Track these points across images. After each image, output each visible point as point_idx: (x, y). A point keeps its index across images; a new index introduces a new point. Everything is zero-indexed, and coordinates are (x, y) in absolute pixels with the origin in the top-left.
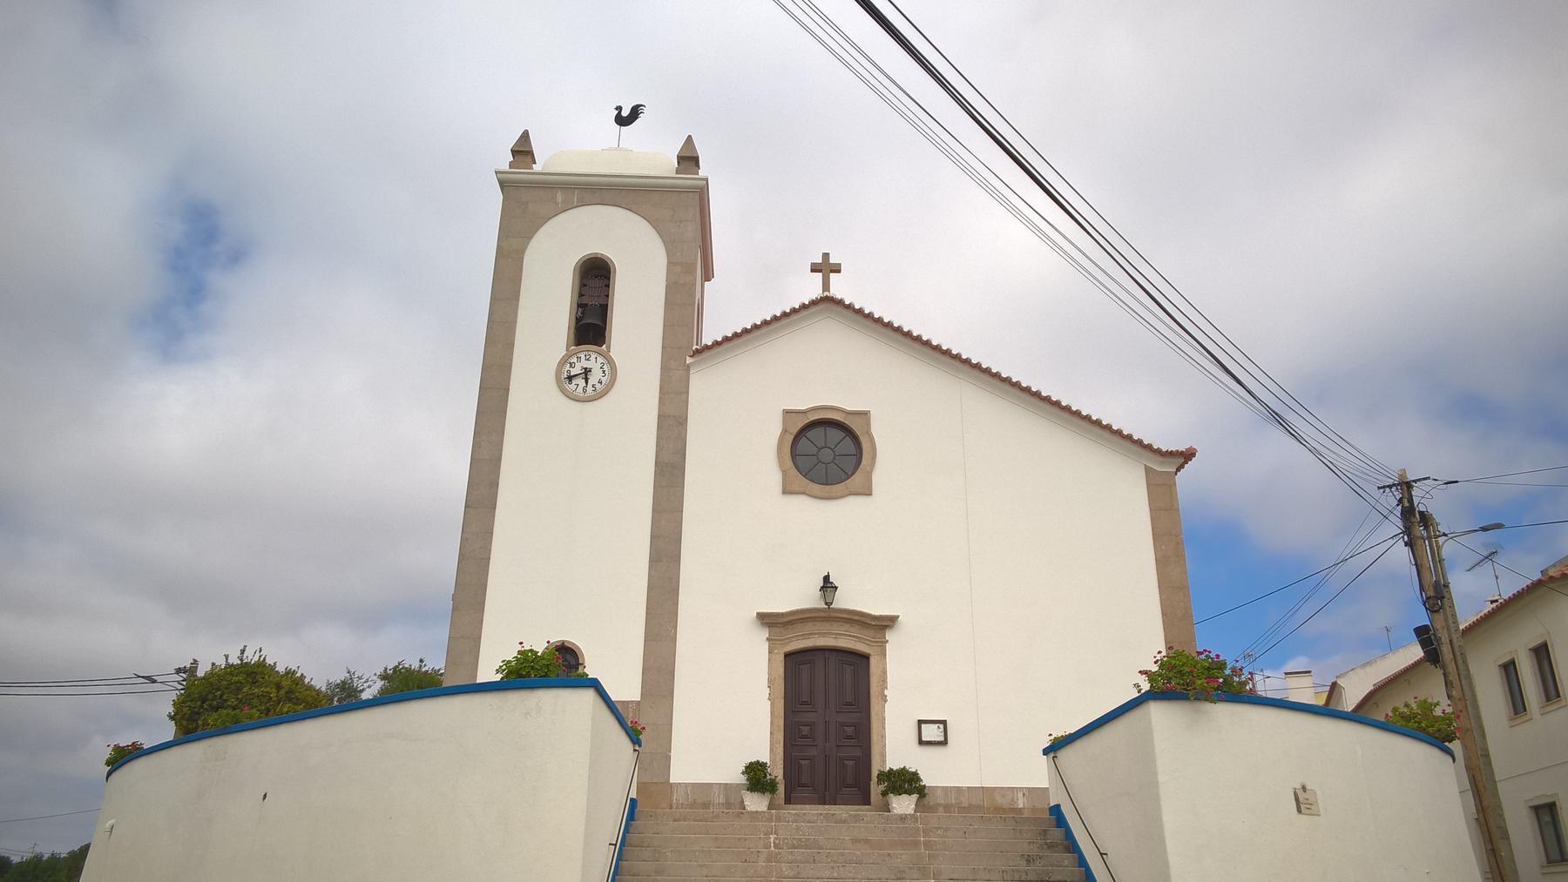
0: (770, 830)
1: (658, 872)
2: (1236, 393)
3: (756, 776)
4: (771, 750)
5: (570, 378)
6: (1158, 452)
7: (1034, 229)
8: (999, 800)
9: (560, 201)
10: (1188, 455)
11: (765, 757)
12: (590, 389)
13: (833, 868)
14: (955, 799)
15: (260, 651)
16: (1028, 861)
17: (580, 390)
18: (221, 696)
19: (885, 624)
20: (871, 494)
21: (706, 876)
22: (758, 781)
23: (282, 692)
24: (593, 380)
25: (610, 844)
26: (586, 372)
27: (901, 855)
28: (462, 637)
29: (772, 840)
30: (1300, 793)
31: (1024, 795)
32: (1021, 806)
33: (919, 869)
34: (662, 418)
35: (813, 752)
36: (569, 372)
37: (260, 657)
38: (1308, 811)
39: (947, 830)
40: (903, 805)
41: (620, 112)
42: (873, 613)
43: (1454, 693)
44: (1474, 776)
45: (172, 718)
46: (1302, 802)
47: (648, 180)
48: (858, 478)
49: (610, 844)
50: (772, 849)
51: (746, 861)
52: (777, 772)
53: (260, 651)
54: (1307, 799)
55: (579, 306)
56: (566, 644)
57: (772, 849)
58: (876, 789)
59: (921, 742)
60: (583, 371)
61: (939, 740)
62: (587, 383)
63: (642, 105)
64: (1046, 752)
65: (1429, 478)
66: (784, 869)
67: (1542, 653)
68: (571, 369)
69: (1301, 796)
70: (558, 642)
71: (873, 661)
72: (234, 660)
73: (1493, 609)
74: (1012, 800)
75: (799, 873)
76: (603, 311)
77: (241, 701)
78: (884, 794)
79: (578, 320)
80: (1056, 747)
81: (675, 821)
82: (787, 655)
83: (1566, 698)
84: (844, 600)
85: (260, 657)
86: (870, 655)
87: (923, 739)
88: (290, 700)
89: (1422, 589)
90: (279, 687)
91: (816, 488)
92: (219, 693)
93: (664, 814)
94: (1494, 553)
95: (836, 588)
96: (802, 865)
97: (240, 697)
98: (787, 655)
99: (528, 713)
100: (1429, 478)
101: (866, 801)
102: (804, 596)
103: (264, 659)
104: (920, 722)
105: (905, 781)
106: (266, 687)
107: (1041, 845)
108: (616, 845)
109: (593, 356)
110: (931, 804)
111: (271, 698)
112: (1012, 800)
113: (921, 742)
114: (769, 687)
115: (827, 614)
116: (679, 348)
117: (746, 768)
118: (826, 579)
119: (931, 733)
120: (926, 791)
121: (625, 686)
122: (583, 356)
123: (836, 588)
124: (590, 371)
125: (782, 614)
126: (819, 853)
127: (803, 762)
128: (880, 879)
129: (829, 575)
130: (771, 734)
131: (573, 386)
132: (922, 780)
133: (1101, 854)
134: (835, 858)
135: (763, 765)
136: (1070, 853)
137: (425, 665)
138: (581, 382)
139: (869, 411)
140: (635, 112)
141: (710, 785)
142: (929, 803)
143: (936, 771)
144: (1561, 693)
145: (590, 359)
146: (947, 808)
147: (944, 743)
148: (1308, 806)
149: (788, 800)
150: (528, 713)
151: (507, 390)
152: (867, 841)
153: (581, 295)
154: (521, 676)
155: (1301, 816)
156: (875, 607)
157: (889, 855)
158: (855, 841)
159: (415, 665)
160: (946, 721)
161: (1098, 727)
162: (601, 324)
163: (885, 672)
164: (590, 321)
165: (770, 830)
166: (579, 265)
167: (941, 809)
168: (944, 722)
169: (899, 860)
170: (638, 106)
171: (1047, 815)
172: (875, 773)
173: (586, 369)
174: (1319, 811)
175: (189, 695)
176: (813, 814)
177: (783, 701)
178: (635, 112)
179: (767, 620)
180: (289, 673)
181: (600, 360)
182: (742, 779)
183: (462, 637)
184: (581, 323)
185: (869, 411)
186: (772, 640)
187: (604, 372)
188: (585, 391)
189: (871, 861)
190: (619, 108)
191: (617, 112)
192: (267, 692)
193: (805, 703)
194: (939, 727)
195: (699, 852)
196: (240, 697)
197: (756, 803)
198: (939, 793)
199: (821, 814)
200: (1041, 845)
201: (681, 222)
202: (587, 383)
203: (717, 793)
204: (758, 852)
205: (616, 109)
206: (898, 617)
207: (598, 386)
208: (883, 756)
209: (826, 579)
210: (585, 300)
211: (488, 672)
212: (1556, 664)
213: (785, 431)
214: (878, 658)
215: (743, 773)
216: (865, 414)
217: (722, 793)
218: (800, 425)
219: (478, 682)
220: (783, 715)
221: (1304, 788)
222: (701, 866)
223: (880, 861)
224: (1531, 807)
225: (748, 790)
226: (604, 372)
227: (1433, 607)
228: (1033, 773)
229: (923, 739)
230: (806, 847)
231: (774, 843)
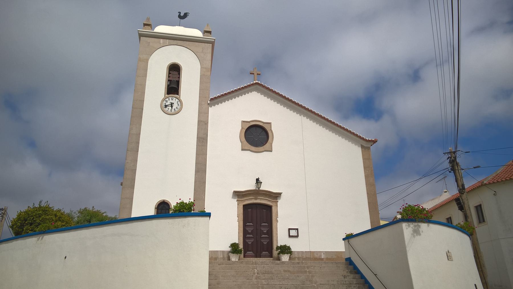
0: (254, 268)
1: (218, 284)
3: (234, 248)
4: (239, 239)
5: (166, 106)
6: (366, 140)
7: (435, 34)
8: (316, 256)
9: (162, 43)
10: (375, 142)
11: (237, 242)
12: (173, 110)
13: (280, 281)
14: (301, 255)
15: (47, 202)
16: (344, 277)
17: (169, 110)
18: (33, 219)
19: (276, 196)
20: (271, 151)
21: (235, 285)
22: (236, 250)
23: (57, 217)
24: (175, 106)
26: (172, 104)
27: (302, 276)
28: (126, 198)
29: (256, 271)
30: (448, 253)
31: (324, 254)
32: (323, 257)
33: (310, 281)
34: (199, 122)
37: (47, 204)
39: (315, 266)
40: (285, 258)
41: (180, 14)
42: (274, 192)
43: (469, 220)
44: (476, 248)
45: (459, 210)
46: (449, 257)
47: (191, 38)
48: (267, 145)
50: (256, 274)
51: (248, 279)
52: (241, 246)
53: (47, 202)
54: (450, 255)
55: (169, 80)
56: (165, 201)
57: (256, 274)
58: (275, 253)
59: (290, 236)
60: (171, 103)
61: (295, 235)
62: (172, 108)
63: (188, 13)
64: (344, 239)
65: (460, 151)
66: (263, 282)
68: (166, 103)
69: (448, 254)
70: (162, 200)
71: (274, 208)
72: (37, 206)
74: (320, 255)
75: (268, 283)
76: (178, 83)
77: (41, 221)
78: (279, 254)
79: (168, 86)
80: (348, 238)
81: (219, 265)
82: (244, 206)
83: (487, 222)
84: (264, 187)
85: (47, 204)
86: (272, 206)
87: (291, 235)
88: (60, 221)
89: (458, 186)
90: (56, 216)
91: (253, 148)
92: (32, 218)
93: (215, 263)
94: (445, 177)
95: (262, 183)
96: (269, 280)
97: (40, 219)
98: (244, 206)
99: (184, 226)
100: (460, 151)
101: (271, 256)
102: (251, 186)
103: (49, 205)
104: (289, 229)
105: (285, 249)
106: (51, 215)
107: (347, 272)
109: (174, 99)
110: (293, 257)
111: (53, 220)
112: (320, 255)
113: (290, 236)
114: (238, 217)
115: (257, 192)
116: (205, 97)
117: (231, 245)
118: (257, 180)
119: (293, 233)
120: (293, 253)
122: (171, 99)
123: (262, 183)
124: (173, 104)
125: (243, 191)
126: (274, 276)
128: (297, 285)
130: (238, 233)
131: (167, 109)
132: (291, 249)
133: (375, 275)
134: (279, 278)
135: (238, 244)
136: (357, 274)
137: (95, 209)
138: (170, 108)
139: (271, 123)
140: (186, 15)
141: (217, 251)
142: (292, 257)
143: (296, 246)
144: (486, 221)
145: (172, 99)
146: (299, 258)
149: (244, 257)
150: (184, 226)
151: (143, 109)
152: (289, 271)
153: (169, 77)
154: (181, 212)
155: (449, 261)
156: (274, 190)
157: (298, 276)
158: (285, 271)
159: (91, 209)
160: (298, 229)
161: (29, 236)
162: (176, 87)
163: (277, 212)
164: (173, 86)
165: (254, 268)
167: (297, 259)
168: (297, 229)
169: (301, 278)
170: (187, 13)
171: (344, 261)
172: (275, 247)
173: (172, 103)
174: (453, 259)
175: (19, 219)
176: (268, 262)
177: (243, 222)
178: (186, 15)
179: (238, 195)
180: (59, 211)
181: (177, 100)
182: (229, 249)
183: (126, 198)
185: (271, 123)
186: (239, 200)
187: (178, 104)
188: (171, 111)
189: (292, 278)
190: (180, 13)
191: (179, 14)
192: (52, 218)
194: (296, 231)
195: (231, 276)
196: (40, 219)
197: (234, 258)
198: (296, 253)
199: (271, 262)
200: (347, 272)
201: (205, 53)
202: (172, 108)
203: (220, 254)
204: (252, 276)
205: (179, 12)
206: (282, 193)
207: (176, 109)
208: (277, 241)
209: (257, 180)
210: (170, 79)
212: (484, 211)
213: (242, 128)
214: (275, 207)
215: (229, 247)
216: (270, 123)
217: (221, 254)
218: (248, 126)
219: (132, 217)
220: (243, 226)
221: (448, 251)
222: (234, 281)
223: (295, 278)
225: (232, 253)
226: (178, 104)
227: (462, 192)
228: (340, 247)
229: (291, 235)
230: (268, 274)
231: (257, 272)
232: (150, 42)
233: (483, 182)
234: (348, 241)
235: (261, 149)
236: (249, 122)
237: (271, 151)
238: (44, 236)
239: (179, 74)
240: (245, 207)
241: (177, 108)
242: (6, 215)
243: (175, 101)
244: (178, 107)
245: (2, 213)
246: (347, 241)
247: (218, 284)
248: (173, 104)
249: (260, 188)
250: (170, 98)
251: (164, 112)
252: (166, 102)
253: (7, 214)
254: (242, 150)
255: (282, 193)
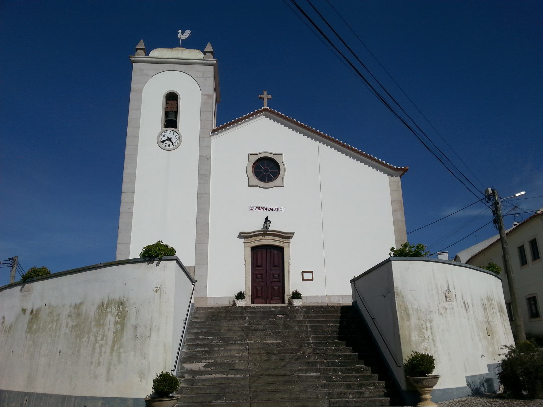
2: (279, 241)
12: (174, 144)
19: (288, 236)
24: (173, 140)
25: (184, 320)
35: (262, 284)
36: (162, 138)
38: (450, 301)
49: (184, 320)
54: (449, 296)
67: (534, 243)
68: (163, 137)
71: (286, 250)
73: (515, 228)
74: (338, 300)
76: (176, 113)
87: (311, 273)
91: (262, 184)
95: (271, 222)
104: (303, 272)
108: (186, 320)
109: (172, 132)
118: (267, 219)
119: (307, 276)
121: (188, 261)
122: (168, 133)
123: (271, 222)
127: (258, 288)
129: (268, 217)
131: (164, 144)
133: (372, 319)
139: (283, 154)
143: (306, 290)
145: (171, 133)
147: (312, 280)
148: (450, 299)
155: (447, 302)
166: (165, 95)
168: (312, 272)
179: (243, 236)
181: (175, 134)
184: (168, 119)
193: (259, 266)
209: (267, 219)
211: (135, 253)
224: (527, 298)
229: (311, 273)
232: (143, 70)
233: (536, 213)
234: (354, 283)
235: (271, 184)
236: (257, 154)
237: (283, 186)
238: (26, 285)
239: (177, 104)
240: (253, 249)
241: (176, 143)
242: (17, 264)
243: (173, 135)
244: (177, 142)
245: (12, 263)
246: (353, 282)
247: (105, 325)
248: (171, 138)
249: (269, 228)
250: (168, 132)
251: (160, 147)
252: (163, 136)
253: (18, 264)
254: (249, 186)
255: (294, 233)
